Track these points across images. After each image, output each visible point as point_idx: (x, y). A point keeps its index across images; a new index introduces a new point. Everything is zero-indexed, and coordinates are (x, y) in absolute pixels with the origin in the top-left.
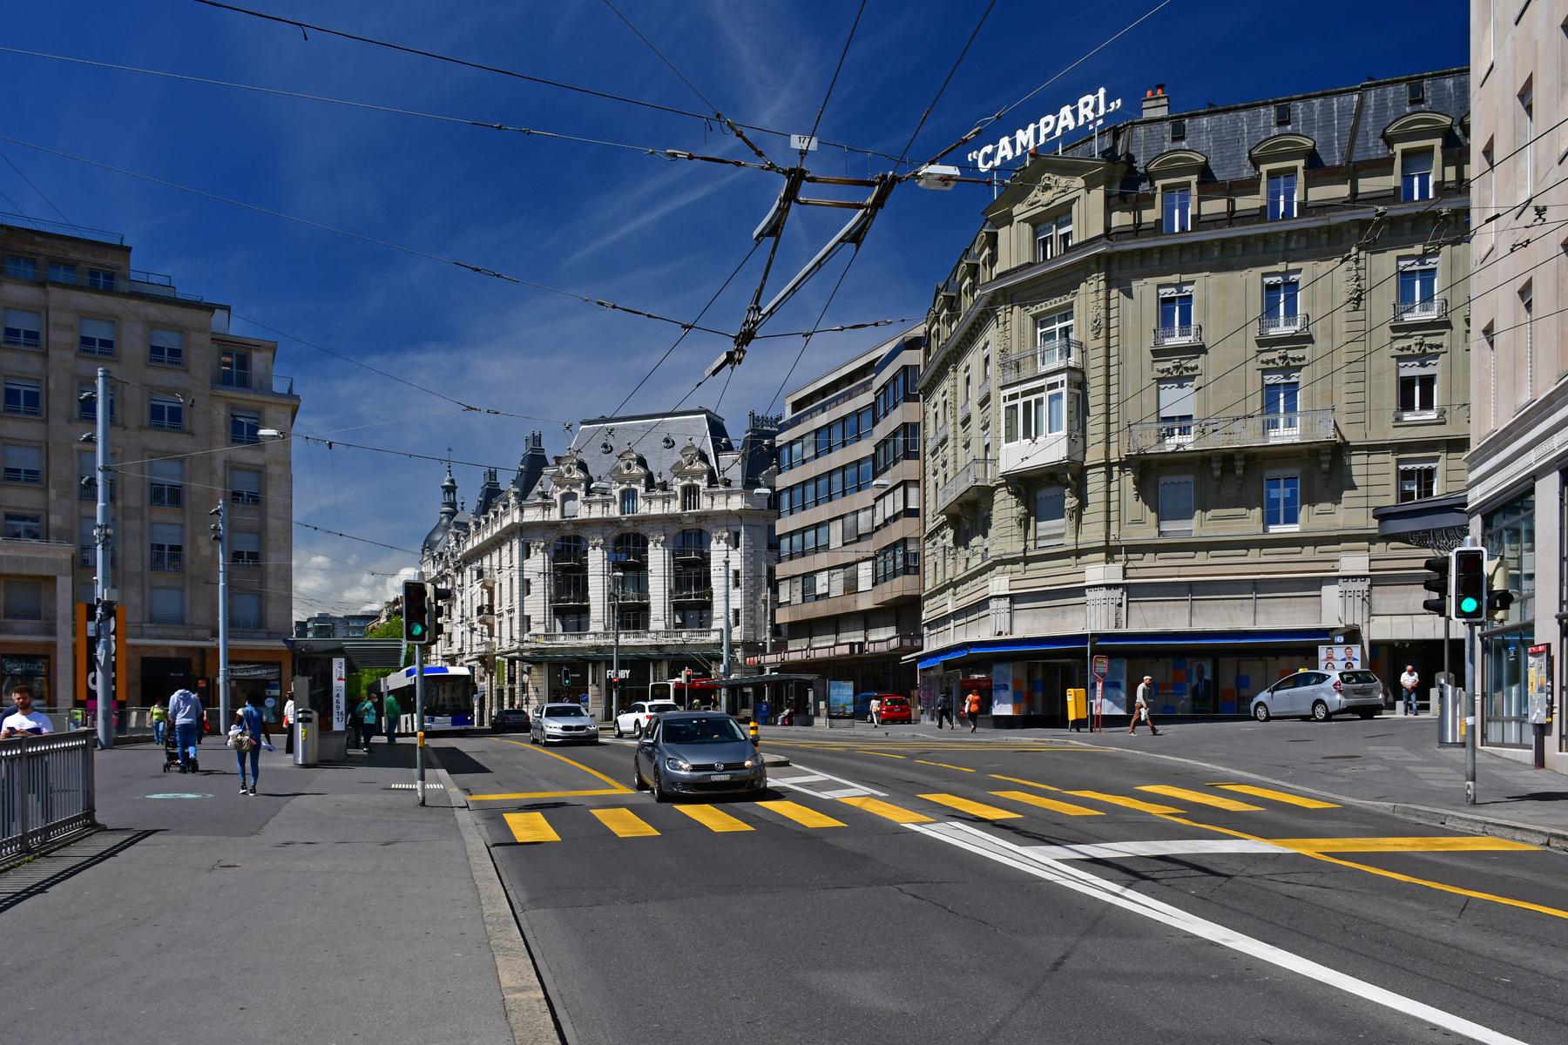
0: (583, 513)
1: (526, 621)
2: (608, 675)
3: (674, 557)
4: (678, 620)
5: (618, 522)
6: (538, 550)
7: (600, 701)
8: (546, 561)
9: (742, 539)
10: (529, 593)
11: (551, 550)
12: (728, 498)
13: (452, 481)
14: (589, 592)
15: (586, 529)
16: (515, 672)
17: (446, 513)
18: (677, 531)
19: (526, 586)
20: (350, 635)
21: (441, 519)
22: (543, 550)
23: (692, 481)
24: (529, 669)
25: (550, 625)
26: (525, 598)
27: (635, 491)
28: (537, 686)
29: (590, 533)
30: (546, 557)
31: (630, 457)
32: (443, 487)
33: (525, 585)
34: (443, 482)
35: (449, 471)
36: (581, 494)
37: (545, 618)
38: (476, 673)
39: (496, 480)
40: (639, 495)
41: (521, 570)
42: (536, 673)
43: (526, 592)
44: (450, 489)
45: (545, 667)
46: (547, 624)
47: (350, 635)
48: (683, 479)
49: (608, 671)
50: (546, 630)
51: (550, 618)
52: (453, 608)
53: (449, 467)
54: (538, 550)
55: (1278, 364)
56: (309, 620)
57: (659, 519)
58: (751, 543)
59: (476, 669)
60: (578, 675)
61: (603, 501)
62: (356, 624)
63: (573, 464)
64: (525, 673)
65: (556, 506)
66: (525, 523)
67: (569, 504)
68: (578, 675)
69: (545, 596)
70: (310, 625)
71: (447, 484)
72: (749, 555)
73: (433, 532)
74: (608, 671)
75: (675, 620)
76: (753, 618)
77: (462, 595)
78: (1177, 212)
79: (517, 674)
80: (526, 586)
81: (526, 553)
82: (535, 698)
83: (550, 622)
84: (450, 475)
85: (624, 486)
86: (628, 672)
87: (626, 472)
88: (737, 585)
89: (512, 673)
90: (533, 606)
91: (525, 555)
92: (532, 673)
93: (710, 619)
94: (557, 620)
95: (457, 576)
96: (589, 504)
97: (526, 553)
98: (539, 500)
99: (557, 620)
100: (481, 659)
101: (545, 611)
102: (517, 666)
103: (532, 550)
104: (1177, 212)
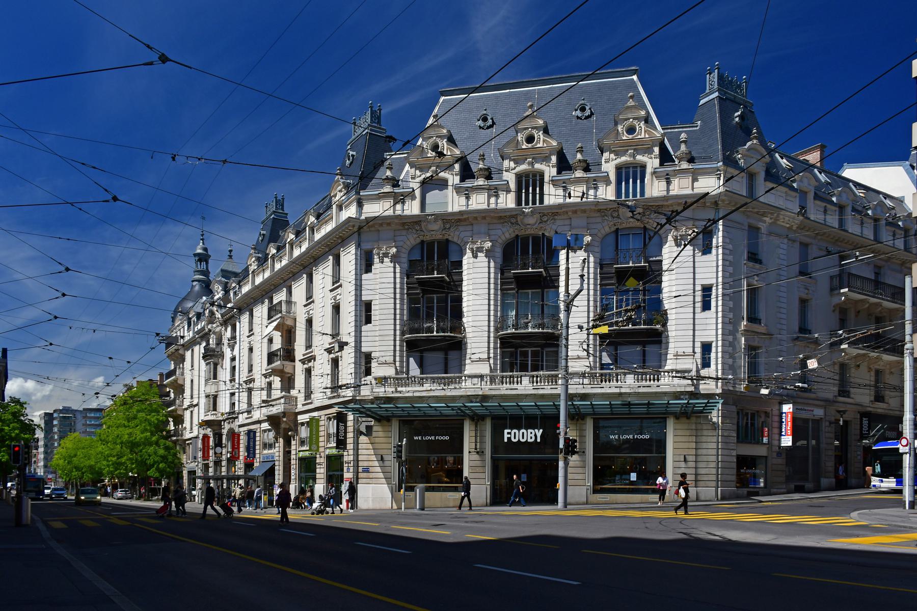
0: (454, 203)
1: (365, 362)
2: (506, 436)
3: (601, 268)
4: (606, 359)
5: (515, 216)
6: (386, 260)
7: (482, 476)
8: (398, 275)
9: (718, 239)
10: (368, 321)
11: (404, 259)
12: (695, 180)
13: (205, 249)
14: (464, 320)
15: (461, 228)
16: (346, 433)
17: (198, 281)
18: (607, 230)
19: (365, 312)
20: (88, 423)
21: (193, 287)
22: (395, 259)
23: (634, 157)
24: (369, 429)
25: (402, 367)
26: (364, 328)
27: (542, 174)
28: (381, 452)
29: (469, 234)
30: (398, 270)
31: (534, 124)
32: (195, 255)
33: (363, 309)
34: (196, 250)
35: (202, 240)
36: (453, 179)
37: (395, 356)
38: (258, 439)
39: (283, 209)
40: (546, 179)
41: (359, 287)
42: (381, 434)
43: (364, 319)
44: (203, 258)
45: (395, 424)
46: (398, 364)
47: (88, 423)
48: (618, 154)
49: (506, 431)
50: (397, 373)
51: (401, 356)
52: (219, 367)
53: (202, 235)
54: (386, 260)
55: (112, 461)
56: (55, 411)
57: (584, 211)
58: (730, 247)
59: (258, 434)
60: (447, 438)
61: (489, 189)
62: (93, 415)
63: (441, 137)
64: (361, 433)
65: (413, 198)
66: (368, 220)
67: (433, 196)
68: (447, 438)
69: (395, 325)
70: (55, 415)
71: (199, 251)
72: (728, 263)
73: (185, 299)
74: (506, 431)
75: (601, 359)
76: (732, 356)
77: (232, 350)
78: (623, 183)
79: (350, 435)
80: (365, 312)
81: (365, 263)
82: (379, 469)
83: (401, 362)
84: (203, 243)
85: (523, 167)
86: (539, 433)
87: (525, 146)
88: (706, 306)
89: (342, 433)
90: (377, 339)
91: (364, 267)
92: (374, 434)
93: (661, 359)
94: (411, 360)
95: (226, 330)
96: (467, 193)
97: (365, 263)
98: (387, 189)
99: (411, 360)
100: (274, 420)
101: (395, 346)
102: (350, 423)
103: (376, 260)
104: (623, 183)
